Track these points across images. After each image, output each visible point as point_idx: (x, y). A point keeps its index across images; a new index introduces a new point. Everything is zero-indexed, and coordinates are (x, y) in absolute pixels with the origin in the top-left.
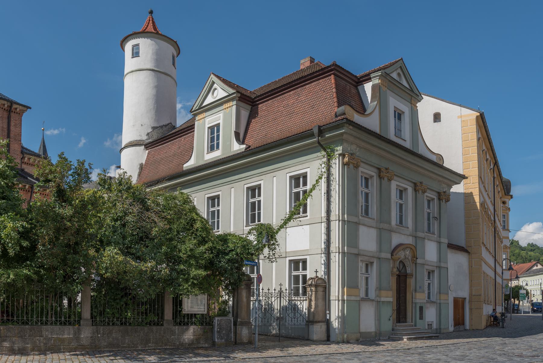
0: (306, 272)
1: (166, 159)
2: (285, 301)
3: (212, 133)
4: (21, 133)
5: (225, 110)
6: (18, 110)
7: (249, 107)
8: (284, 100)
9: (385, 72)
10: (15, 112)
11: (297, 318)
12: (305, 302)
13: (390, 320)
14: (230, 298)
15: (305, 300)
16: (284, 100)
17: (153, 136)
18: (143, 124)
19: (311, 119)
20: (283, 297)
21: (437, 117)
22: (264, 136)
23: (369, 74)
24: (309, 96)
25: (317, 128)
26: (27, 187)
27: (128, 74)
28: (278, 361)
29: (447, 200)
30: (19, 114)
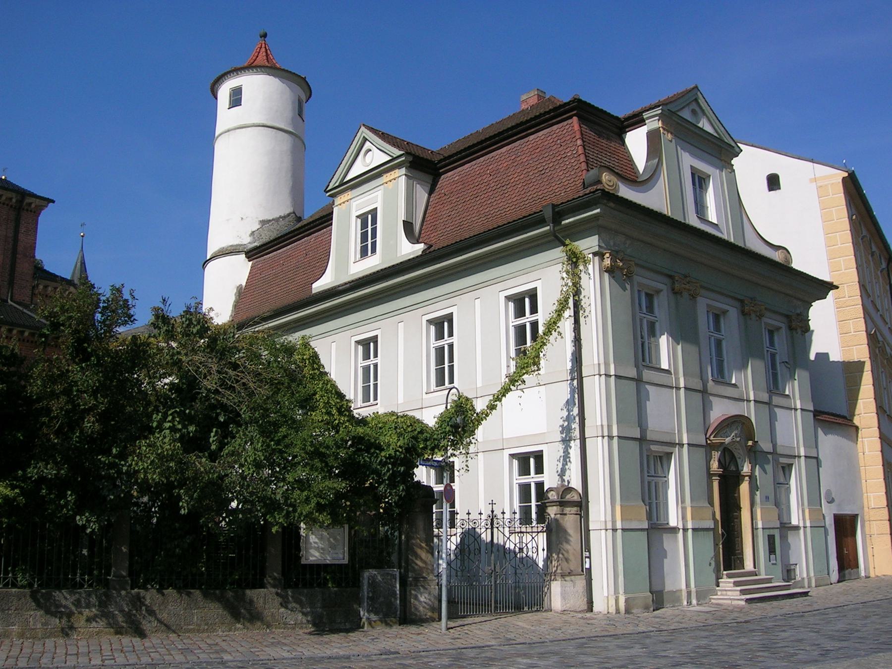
0: (543, 477)
1: (281, 276)
2: (501, 535)
3: (364, 225)
4: (36, 243)
5: (386, 185)
6: (33, 206)
7: (431, 177)
8: (490, 163)
9: (668, 110)
10: (27, 210)
12: (541, 534)
13: (710, 564)
14: (394, 532)
15: (541, 532)
16: (490, 163)
17: (261, 236)
18: (244, 217)
19: (540, 193)
20: (497, 528)
21: (773, 182)
22: (457, 226)
23: (640, 113)
24: (536, 155)
25: (550, 209)
27: (220, 135)
28: (484, 655)
29: (804, 330)
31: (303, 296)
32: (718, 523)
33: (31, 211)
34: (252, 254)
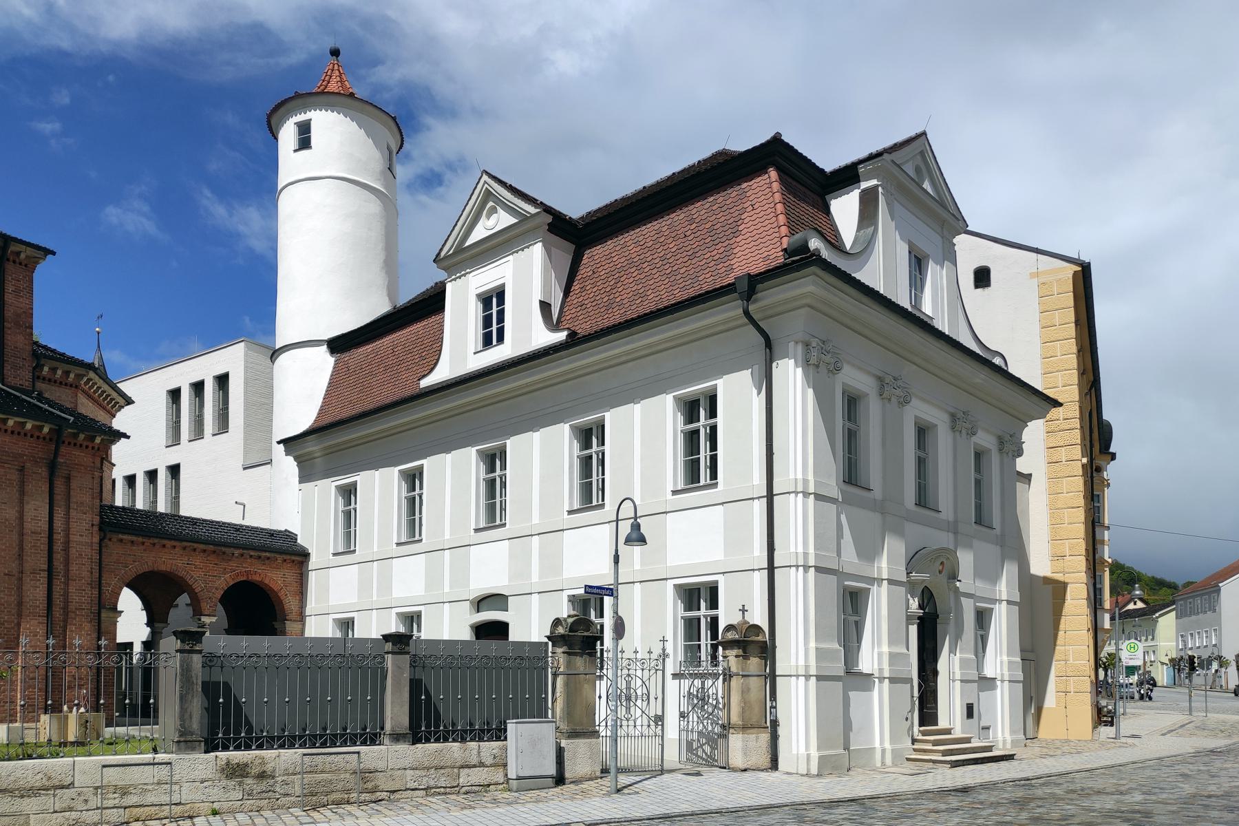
6: (23, 256)
10: (14, 262)
11: (633, 718)
21: (982, 277)
26: (46, 430)
30: (26, 266)
31: (408, 393)
32: (384, 677)
33: (20, 264)
34: (338, 345)
